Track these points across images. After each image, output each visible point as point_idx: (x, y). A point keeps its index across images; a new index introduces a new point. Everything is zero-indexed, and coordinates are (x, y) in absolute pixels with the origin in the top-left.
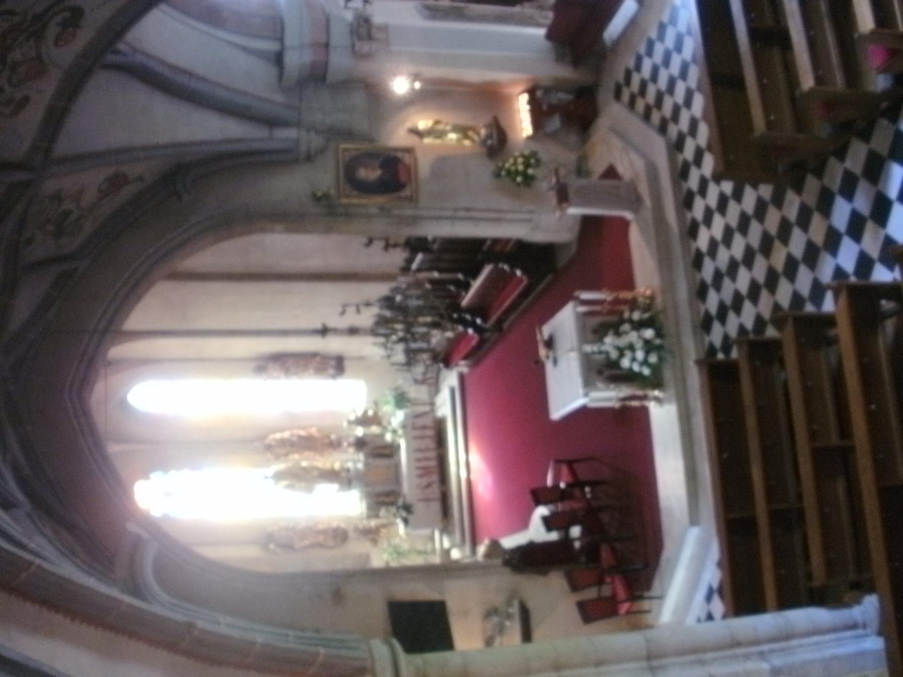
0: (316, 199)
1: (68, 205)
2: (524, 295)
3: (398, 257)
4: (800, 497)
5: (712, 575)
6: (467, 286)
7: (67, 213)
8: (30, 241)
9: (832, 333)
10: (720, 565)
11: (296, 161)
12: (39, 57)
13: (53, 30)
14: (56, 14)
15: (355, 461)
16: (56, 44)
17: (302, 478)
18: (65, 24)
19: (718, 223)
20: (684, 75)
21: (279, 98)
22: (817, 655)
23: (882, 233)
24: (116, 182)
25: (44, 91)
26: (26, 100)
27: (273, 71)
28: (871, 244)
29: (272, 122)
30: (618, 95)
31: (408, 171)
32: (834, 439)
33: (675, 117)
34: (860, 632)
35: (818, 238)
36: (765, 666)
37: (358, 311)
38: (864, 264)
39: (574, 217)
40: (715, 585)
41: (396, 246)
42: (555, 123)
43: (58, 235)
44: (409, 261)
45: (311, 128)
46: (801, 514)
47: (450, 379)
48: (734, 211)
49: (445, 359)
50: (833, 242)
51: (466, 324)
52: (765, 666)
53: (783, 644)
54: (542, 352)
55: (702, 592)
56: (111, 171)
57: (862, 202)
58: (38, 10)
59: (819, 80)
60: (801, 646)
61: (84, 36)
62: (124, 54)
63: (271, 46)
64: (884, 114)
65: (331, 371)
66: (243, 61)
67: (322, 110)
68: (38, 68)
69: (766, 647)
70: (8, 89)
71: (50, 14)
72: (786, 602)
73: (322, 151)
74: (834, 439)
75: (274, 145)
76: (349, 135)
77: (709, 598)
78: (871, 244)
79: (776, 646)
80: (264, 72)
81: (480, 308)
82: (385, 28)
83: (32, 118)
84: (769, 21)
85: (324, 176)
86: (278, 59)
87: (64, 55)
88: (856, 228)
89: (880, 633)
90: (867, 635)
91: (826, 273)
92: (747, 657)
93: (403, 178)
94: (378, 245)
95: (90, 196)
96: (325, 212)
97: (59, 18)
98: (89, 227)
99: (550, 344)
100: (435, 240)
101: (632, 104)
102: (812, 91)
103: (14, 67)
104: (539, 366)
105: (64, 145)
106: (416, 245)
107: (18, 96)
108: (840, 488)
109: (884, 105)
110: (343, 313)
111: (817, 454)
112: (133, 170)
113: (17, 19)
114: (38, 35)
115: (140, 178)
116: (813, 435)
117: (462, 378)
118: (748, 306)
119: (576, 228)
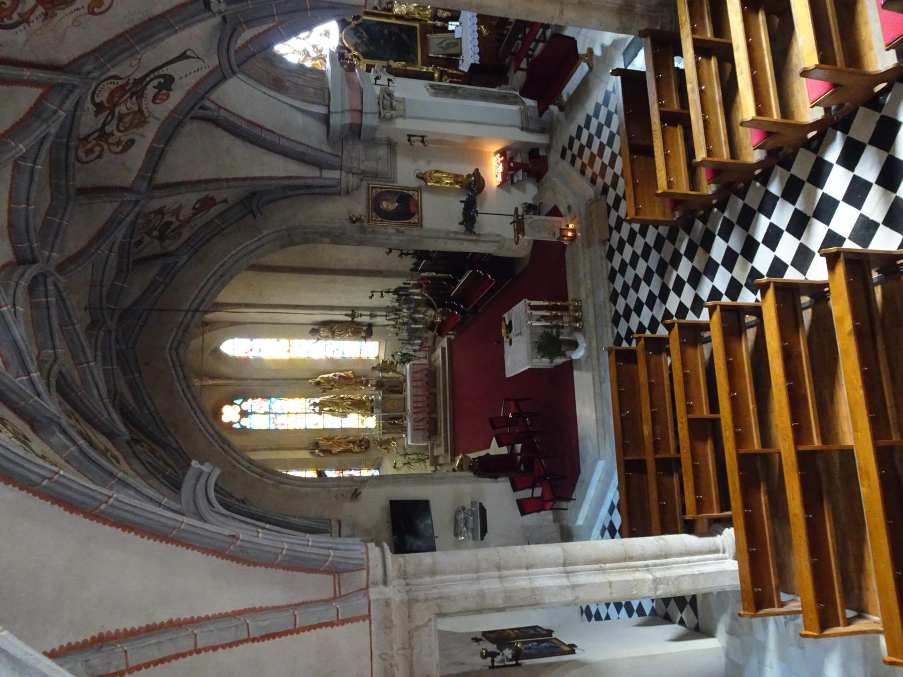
0: (353, 221)
1: (168, 218)
2: (492, 291)
3: (409, 262)
4: (678, 450)
5: (613, 495)
6: (455, 283)
7: (169, 224)
8: (140, 242)
9: (706, 335)
10: (618, 488)
11: (339, 194)
12: (140, 111)
13: (150, 91)
14: (155, 78)
15: (377, 396)
16: (154, 102)
17: (339, 407)
18: (159, 87)
19: (628, 250)
20: (610, 143)
21: (326, 148)
22: (688, 571)
23: (750, 265)
24: (207, 203)
25: (147, 136)
26: (132, 141)
27: (323, 128)
28: (741, 273)
29: (320, 165)
30: (563, 156)
31: (417, 205)
32: (705, 413)
33: (603, 174)
34: (721, 555)
35: (700, 266)
36: (649, 576)
37: (382, 296)
38: (734, 288)
39: (529, 241)
40: (616, 503)
41: (407, 254)
42: (519, 176)
43: (162, 238)
44: (417, 265)
45: (350, 172)
46: (678, 461)
47: (444, 342)
48: (639, 242)
49: (441, 331)
50: (711, 269)
51: (454, 308)
52: (649, 576)
53: (664, 561)
54: (504, 331)
55: (607, 506)
56: (203, 194)
57: (736, 242)
58: (138, 76)
59: (709, 153)
60: (676, 563)
61: (176, 96)
62: (211, 110)
63: (322, 110)
64: (757, 178)
65: (363, 334)
66: (300, 120)
67: (358, 156)
68: (140, 118)
69: (650, 562)
70: (117, 134)
71: (148, 79)
72: (666, 529)
73: (358, 188)
74: (705, 413)
75: (321, 182)
76: (375, 175)
77: (611, 511)
78: (741, 273)
79: (657, 561)
80: (316, 130)
81: (463, 297)
82: (403, 101)
83: (137, 155)
84: (676, 106)
85: (359, 206)
86: (326, 119)
87: (161, 111)
88: (730, 260)
89: (736, 558)
90: (726, 559)
91: (705, 292)
92: (636, 569)
93: (412, 209)
94: (395, 253)
95: (186, 212)
96: (357, 231)
97: (155, 83)
98: (186, 233)
99: (509, 328)
100: (434, 252)
101: (573, 162)
102: (703, 161)
103: (121, 118)
104: (501, 342)
105: (163, 176)
106: (420, 255)
107: (125, 139)
108: (709, 447)
109: (757, 172)
110: (371, 297)
111: (693, 424)
112: (219, 196)
113: (121, 82)
114: (140, 95)
115: (225, 201)
116: (689, 409)
117: (450, 342)
118: (644, 298)
119: (530, 248)
